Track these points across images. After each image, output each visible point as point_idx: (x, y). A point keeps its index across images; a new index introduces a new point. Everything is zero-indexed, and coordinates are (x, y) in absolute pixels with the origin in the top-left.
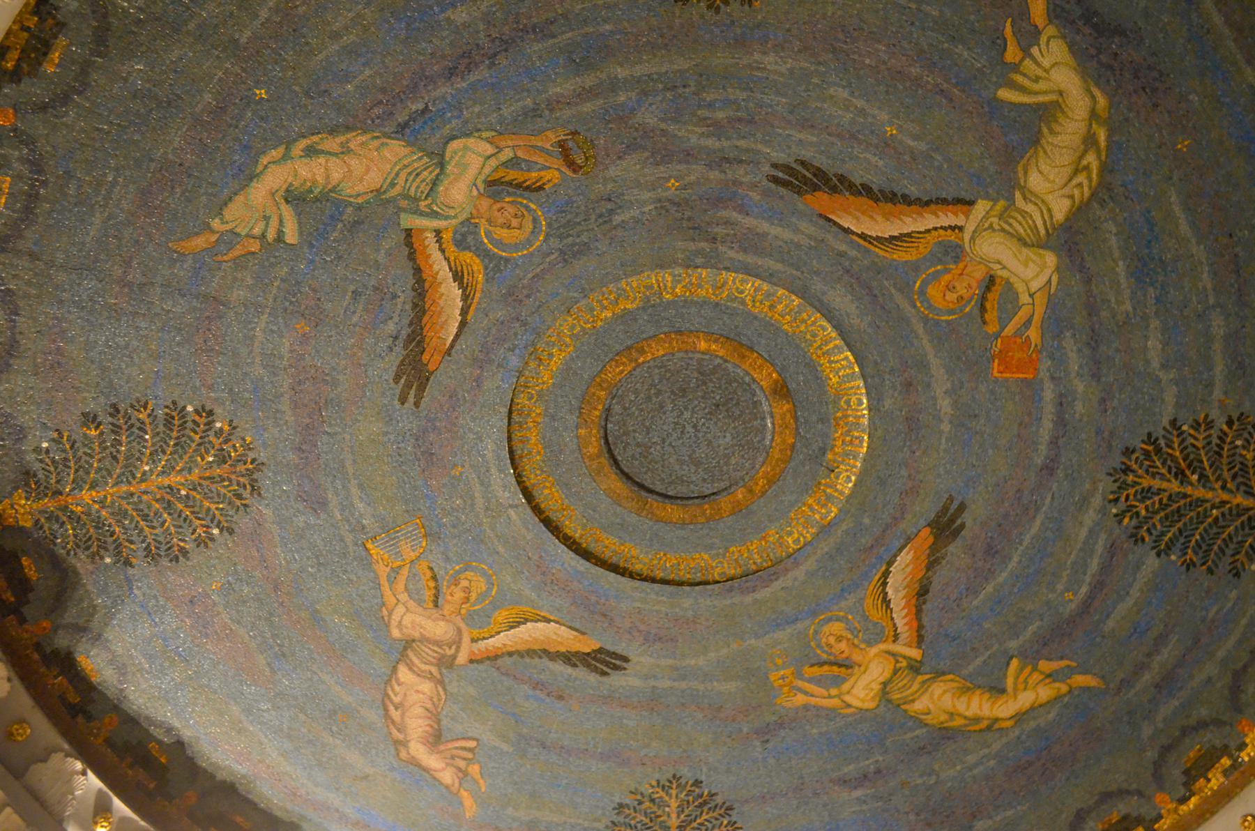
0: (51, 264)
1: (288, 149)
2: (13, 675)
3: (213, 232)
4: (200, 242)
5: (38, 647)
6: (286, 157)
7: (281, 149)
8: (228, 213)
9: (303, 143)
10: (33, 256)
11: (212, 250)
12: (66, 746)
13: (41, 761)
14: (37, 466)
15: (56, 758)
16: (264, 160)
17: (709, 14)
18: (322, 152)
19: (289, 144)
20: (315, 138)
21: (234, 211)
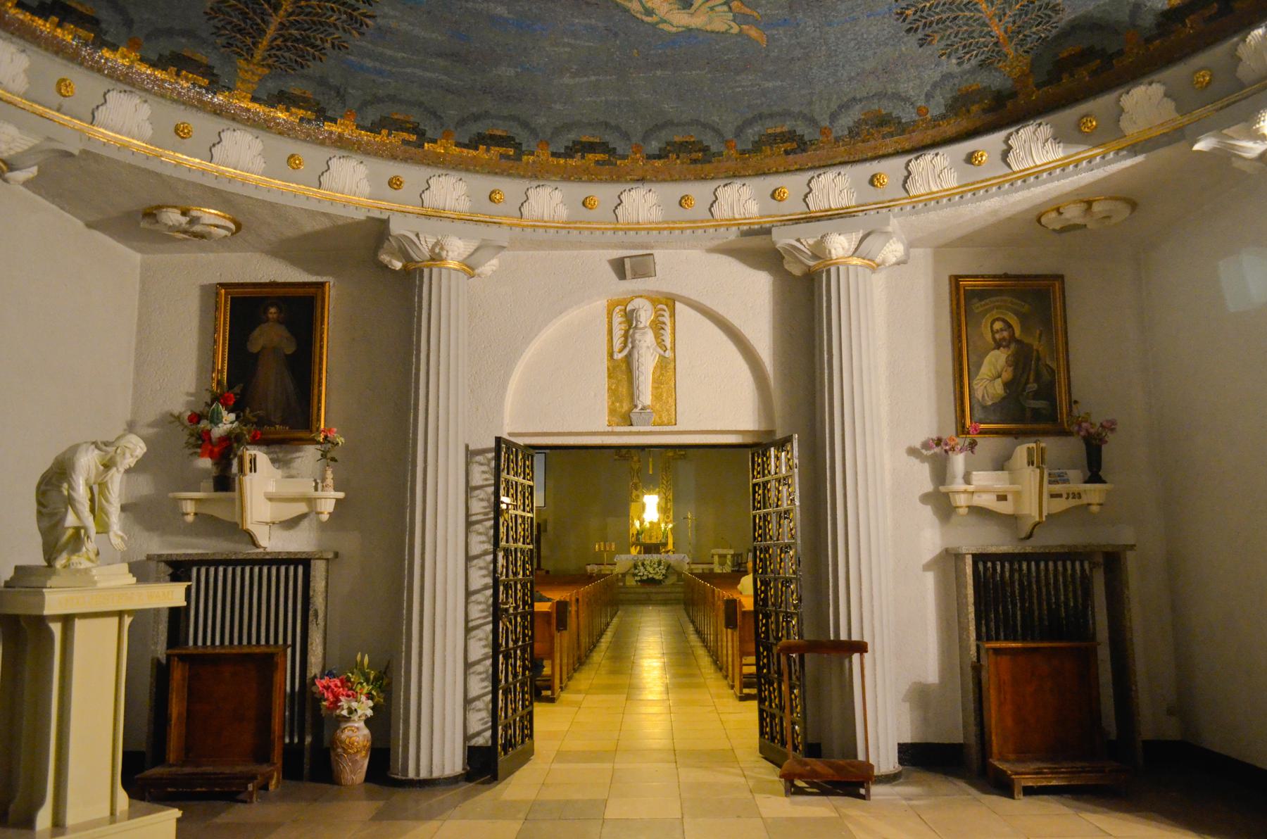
0: (812, 94)
1: (657, 23)
2: (1146, 80)
3: (741, 30)
4: (753, 33)
5: (1148, 40)
6: (663, 21)
7: (661, 26)
8: (723, 28)
9: (648, 19)
10: (810, 103)
11: (755, 23)
12: (1235, 39)
13: (1237, 66)
14: (979, 58)
15: (1242, 51)
16: (674, 30)
17: (90, 546)
18: (644, 7)
19: (654, 25)
20: (638, 15)
21: (719, 26)
